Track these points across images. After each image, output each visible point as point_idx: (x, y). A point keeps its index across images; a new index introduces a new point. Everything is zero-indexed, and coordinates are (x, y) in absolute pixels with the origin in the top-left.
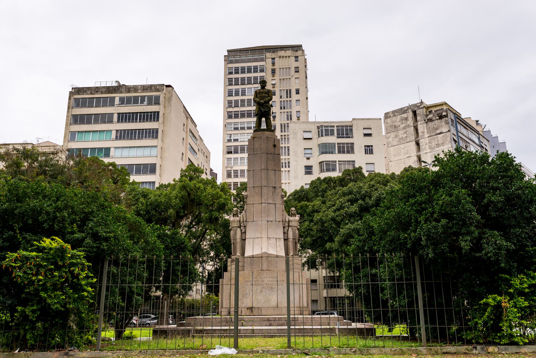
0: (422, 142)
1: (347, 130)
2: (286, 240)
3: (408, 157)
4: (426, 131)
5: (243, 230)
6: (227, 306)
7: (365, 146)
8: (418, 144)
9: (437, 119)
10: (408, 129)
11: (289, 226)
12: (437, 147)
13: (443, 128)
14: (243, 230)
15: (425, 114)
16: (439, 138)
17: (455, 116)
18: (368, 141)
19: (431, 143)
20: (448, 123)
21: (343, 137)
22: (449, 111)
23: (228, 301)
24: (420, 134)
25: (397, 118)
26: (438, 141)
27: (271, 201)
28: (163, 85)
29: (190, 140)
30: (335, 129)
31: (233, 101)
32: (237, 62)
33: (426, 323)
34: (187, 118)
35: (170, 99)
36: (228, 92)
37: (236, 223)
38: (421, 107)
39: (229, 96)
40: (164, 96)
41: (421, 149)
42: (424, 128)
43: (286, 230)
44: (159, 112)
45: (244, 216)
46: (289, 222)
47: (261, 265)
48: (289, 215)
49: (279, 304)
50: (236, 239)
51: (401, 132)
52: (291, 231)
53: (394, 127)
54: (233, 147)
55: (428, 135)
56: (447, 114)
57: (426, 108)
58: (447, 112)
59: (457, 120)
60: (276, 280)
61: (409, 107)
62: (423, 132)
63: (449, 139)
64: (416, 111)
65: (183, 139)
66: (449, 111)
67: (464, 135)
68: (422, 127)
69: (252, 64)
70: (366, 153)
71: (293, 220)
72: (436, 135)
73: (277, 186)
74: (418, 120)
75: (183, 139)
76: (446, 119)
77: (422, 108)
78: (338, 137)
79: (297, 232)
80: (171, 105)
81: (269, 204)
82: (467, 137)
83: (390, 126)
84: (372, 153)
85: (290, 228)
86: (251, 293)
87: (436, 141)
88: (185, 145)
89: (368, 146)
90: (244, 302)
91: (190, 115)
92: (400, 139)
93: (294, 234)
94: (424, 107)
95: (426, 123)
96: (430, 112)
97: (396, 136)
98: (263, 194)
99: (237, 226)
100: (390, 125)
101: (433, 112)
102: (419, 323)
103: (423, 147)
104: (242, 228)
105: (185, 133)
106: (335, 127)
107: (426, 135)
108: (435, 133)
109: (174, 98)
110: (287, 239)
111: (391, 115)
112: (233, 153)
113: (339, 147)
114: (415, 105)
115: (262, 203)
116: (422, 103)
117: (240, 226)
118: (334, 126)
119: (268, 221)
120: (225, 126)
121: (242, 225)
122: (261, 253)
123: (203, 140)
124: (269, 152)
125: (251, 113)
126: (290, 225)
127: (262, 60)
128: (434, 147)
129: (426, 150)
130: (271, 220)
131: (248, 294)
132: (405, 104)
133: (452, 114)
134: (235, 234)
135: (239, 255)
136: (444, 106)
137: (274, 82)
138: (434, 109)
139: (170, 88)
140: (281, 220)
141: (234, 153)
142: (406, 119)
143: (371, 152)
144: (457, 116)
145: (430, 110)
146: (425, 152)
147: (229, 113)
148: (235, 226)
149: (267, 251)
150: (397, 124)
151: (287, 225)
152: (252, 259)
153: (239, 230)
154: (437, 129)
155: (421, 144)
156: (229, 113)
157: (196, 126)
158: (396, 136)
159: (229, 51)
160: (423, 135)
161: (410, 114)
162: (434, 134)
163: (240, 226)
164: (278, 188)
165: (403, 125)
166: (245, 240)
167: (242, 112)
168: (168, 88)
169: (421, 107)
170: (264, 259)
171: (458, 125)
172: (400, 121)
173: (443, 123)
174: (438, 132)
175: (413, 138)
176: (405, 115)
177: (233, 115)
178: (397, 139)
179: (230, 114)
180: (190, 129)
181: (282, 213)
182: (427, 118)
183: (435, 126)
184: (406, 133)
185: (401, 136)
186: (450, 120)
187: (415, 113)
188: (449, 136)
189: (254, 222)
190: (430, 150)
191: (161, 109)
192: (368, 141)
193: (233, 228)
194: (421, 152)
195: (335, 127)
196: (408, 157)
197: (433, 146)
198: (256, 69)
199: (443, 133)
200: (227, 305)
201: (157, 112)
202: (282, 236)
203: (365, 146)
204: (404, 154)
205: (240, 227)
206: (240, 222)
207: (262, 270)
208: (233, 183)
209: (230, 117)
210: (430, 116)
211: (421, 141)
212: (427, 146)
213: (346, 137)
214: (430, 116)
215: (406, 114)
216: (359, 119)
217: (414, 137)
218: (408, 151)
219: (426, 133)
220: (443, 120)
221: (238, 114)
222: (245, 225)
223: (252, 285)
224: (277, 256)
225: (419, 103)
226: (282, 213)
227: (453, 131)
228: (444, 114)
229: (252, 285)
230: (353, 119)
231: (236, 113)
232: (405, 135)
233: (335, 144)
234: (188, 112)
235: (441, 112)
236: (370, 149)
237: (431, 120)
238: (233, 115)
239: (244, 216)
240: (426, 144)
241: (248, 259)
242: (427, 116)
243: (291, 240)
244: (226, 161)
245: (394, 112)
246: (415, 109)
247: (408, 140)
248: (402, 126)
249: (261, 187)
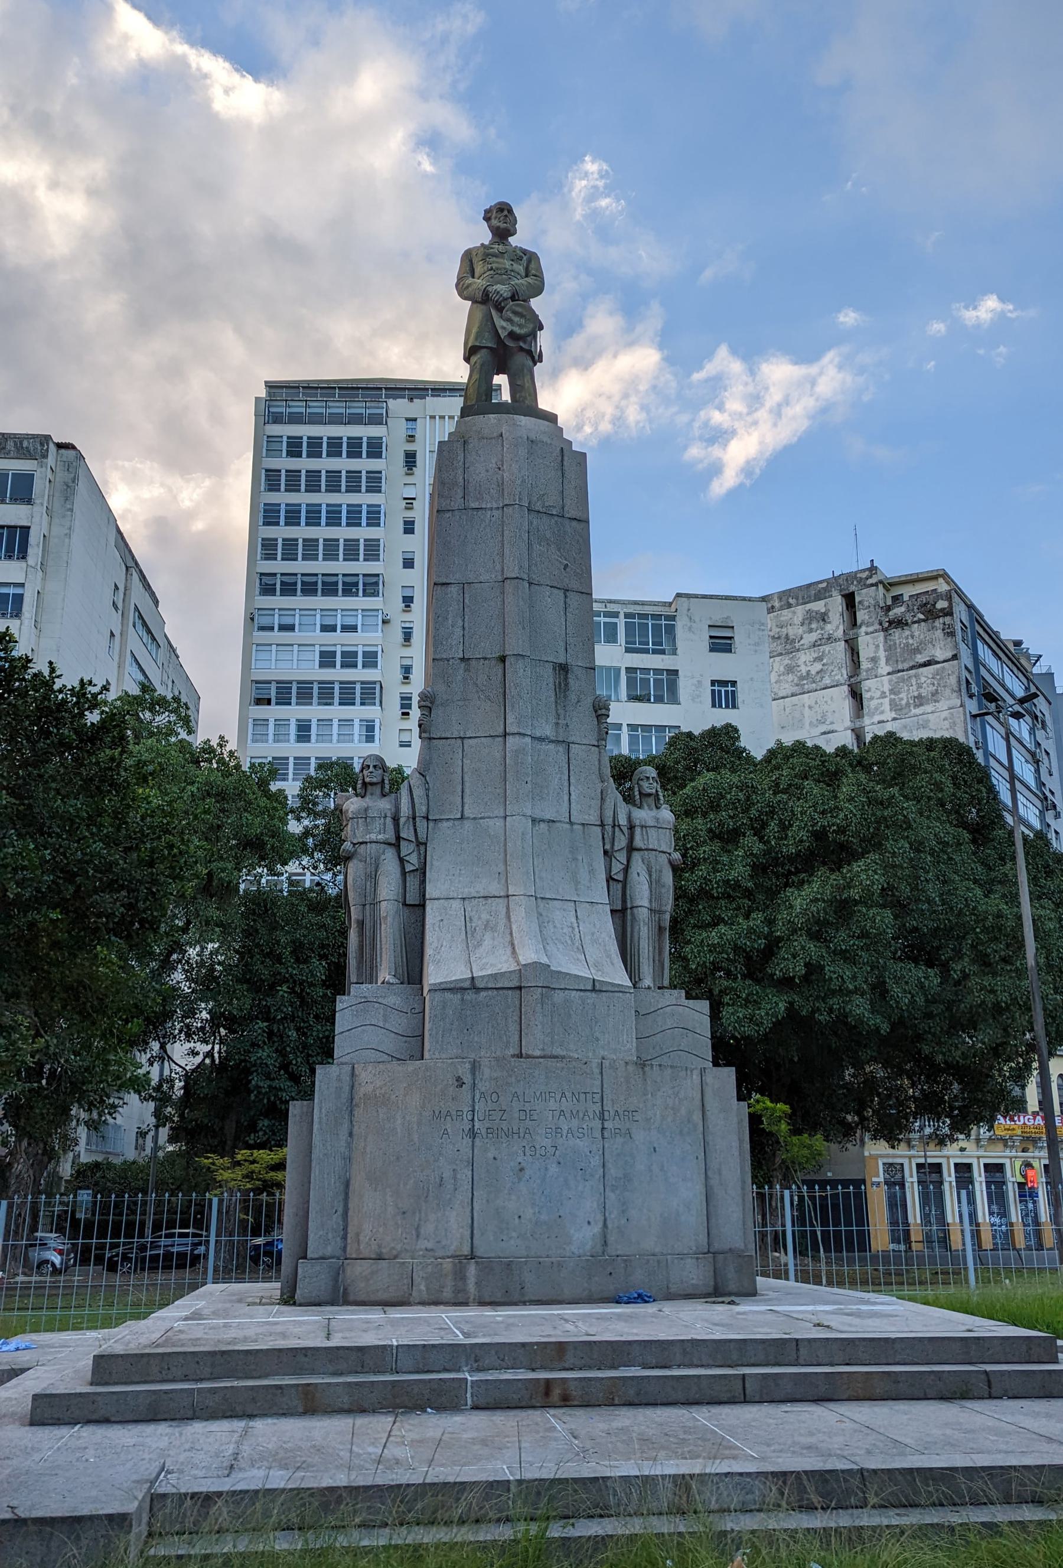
0: (871, 688)
1: (657, 628)
2: (622, 914)
3: (824, 733)
4: (882, 654)
5: (414, 859)
6: (329, 1251)
7: (713, 683)
8: (856, 695)
9: (919, 621)
10: (827, 648)
11: (631, 849)
12: (916, 706)
13: (938, 646)
15: (882, 604)
16: (923, 679)
17: (971, 615)
18: (723, 666)
19: (899, 693)
20: (952, 634)
21: (646, 651)
22: (956, 599)
24: (865, 665)
25: (794, 613)
26: (920, 686)
27: (548, 731)
28: (47, 438)
29: (135, 642)
30: (621, 622)
31: (280, 541)
32: (296, 419)
33: (784, 1232)
34: (127, 568)
35: (69, 490)
36: (265, 511)
37: (377, 824)
38: (870, 581)
39: (266, 524)
40: (49, 475)
41: (866, 710)
42: (878, 646)
43: (617, 868)
44: (29, 528)
46: (632, 828)
47: (513, 1028)
48: (628, 799)
49: (611, 1239)
50: (375, 904)
51: (804, 657)
52: (644, 878)
53: (783, 640)
54: (273, 686)
55: (889, 669)
56: (951, 606)
57: (884, 586)
58: (949, 599)
59: (978, 628)
60: (597, 1108)
61: (834, 582)
62: (874, 660)
63: (953, 680)
64: (853, 594)
65: (112, 635)
66: (956, 599)
67: (992, 675)
68: (870, 644)
69: (345, 432)
71: (651, 822)
72: (912, 668)
73: (576, 662)
74: (859, 621)
75: (112, 635)
76: (948, 620)
77: (872, 585)
78: (628, 650)
79: (668, 878)
80: (72, 510)
81: (540, 739)
82: (999, 683)
83: (773, 637)
84: (734, 707)
85: (636, 856)
87: (915, 687)
88: (116, 657)
90: (428, 1228)
91: (137, 564)
92: (802, 678)
93: (655, 883)
94: (881, 582)
95: (885, 630)
96: (897, 599)
97: (790, 669)
98: (511, 691)
99: (381, 837)
100: (772, 634)
101: (906, 598)
102: (793, 1232)
103: (873, 704)
104: (406, 848)
105: (117, 617)
106: (622, 615)
107: (884, 668)
108: (912, 664)
109: (82, 487)
110: (624, 910)
111: (777, 604)
112: (273, 701)
113: (631, 683)
114: (851, 577)
115: (505, 735)
116: (873, 569)
117: (398, 838)
118: (616, 615)
119: (534, 820)
120: (252, 619)
121: (406, 833)
122: (513, 967)
123: (178, 652)
124: (538, 507)
125: (336, 584)
126: (638, 842)
127: (376, 420)
128: (908, 704)
129: (882, 712)
130: (548, 817)
132: (819, 572)
133: (963, 607)
134: (373, 877)
135: (388, 978)
136: (941, 580)
137: (410, 492)
138: (907, 591)
139: (71, 452)
142: (823, 618)
143: (732, 702)
144: (976, 616)
145: (896, 591)
146: (876, 719)
147: (265, 579)
148: (373, 837)
149: (544, 960)
150: (792, 632)
151: (621, 842)
152: (470, 996)
154: (917, 651)
155: (866, 696)
156: (265, 579)
157: (156, 602)
158: (790, 669)
159: (270, 386)
160: (876, 667)
161: (836, 603)
162: (906, 666)
163: (398, 838)
164: (579, 672)
165: (814, 637)
166: (422, 906)
167: (306, 579)
168: (63, 451)
169: (870, 581)
170: (532, 998)
171: (979, 644)
172: (802, 624)
173: (939, 633)
174: (921, 658)
175: (842, 675)
176: (819, 606)
177: (278, 587)
178: (790, 677)
179: (266, 580)
180: (136, 608)
181: (599, 786)
182: (886, 615)
183: (911, 641)
184: (819, 659)
185: (804, 669)
186: (960, 624)
187: (850, 600)
188: (952, 674)
189: (467, 824)
190: (893, 715)
191: (36, 519)
192: (723, 666)
193: (362, 849)
194: (866, 717)
195: (622, 615)
196: (824, 733)
197: (904, 702)
198: (354, 448)
199: (938, 663)
201: (21, 527)
202: (600, 893)
203: (713, 683)
204: (811, 723)
205: (396, 843)
206: (396, 820)
209: (268, 590)
210: (898, 611)
211: (866, 685)
212: (887, 701)
213: (655, 652)
214: (898, 611)
215: (822, 602)
216: (696, 596)
217: (845, 672)
218: (824, 716)
219: (883, 661)
220: (939, 623)
221: (295, 584)
222: (422, 836)
223: (473, 1134)
224: (595, 987)
225: (864, 570)
227: (966, 659)
228: (942, 604)
229: (473, 1134)
230: (678, 595)
231: (286, 579)
232: (818, 666)
233: (618, 670)
234: (130, 551)
235: (931, 598)
236: (727, 692)
237: (899, 623)
238: (278, 587)
240: (883, 695)
241: (448, 995)
242: (888, 609)
243: (643, 914)
244: (250, 726)
245: (784, 595)
246: (852, 588)
247: (827, 681)
248: (810, 638)
249: (503, 659)
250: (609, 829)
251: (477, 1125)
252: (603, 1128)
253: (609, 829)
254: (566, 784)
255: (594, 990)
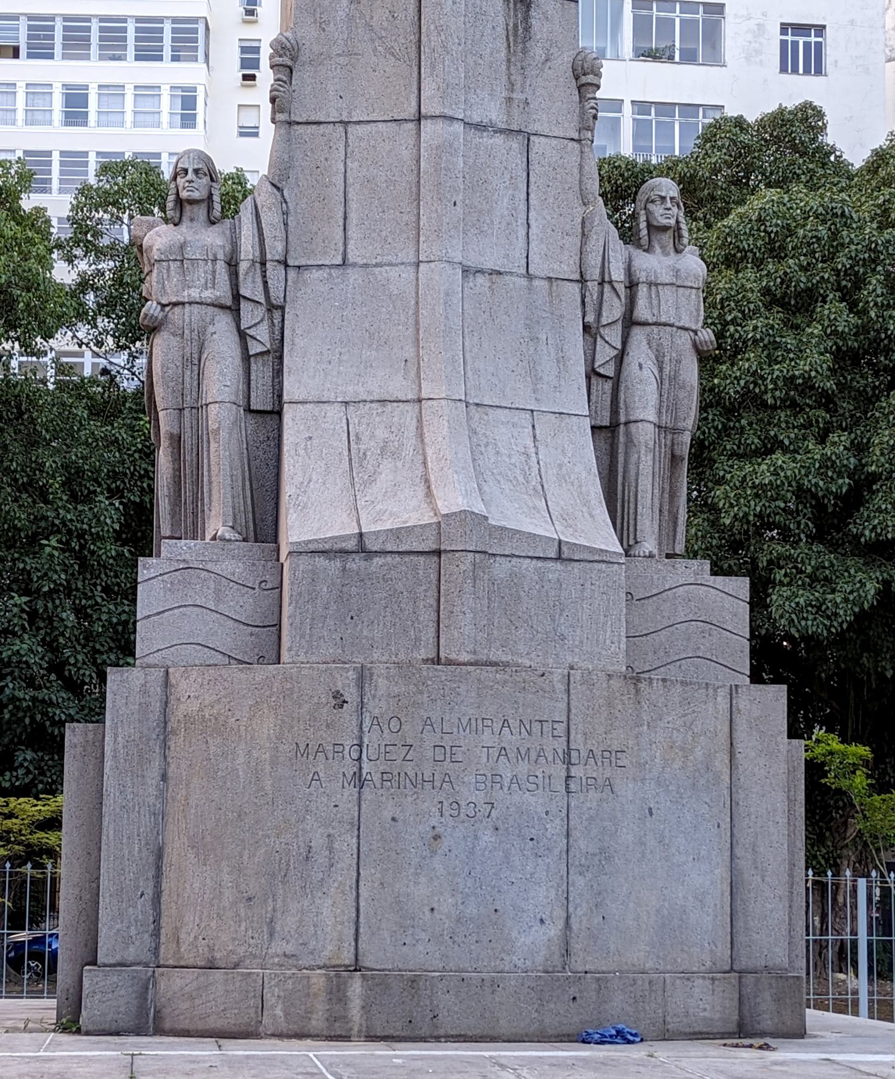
6: (131, 953)
11: (629, 322)
14: (262, 334)
23: (142, 908)
37: (201, 273)
43: (605, 354)
45: (270, 219)
46: (632, 286)
47: (427, 616)
49: (577, 946)
50: (199, 408)
52: (650, 366)
54: (23, 24)
70: (783, 69)
79: (691, 372)
81: (480, 127)
84: (819, 72)
85: (638, 335)
86: (346, 843)
89: (801, 29)
98: (431, 40)
104: (250, 315)
112: (23, 52)
117: (237, 297)
119: (466, 271)
121: (250, 288)
122: (428, 518)
126: (642, 311)
130: (489, 265)
131: (321, 859)
135: (223, 531)
140: (568, 268)
141: (30, 56)
149: (479, 508)
151: (614, 310)
152: (356, 563)
153: (223, 323)
163: (237, 297)
181: (579, 211)
189: (354, 276)
200: (127, 941)
206: (232, 265)
207: (437, 661)
208: (63, 153)
222: (276, 294)
223: (359, 781)
226: (579, 211)
229: (359, 781)
236: (807, 45)
239: (270, 219)
243: (645, 434)
250: (593, 286)
251: (366, 767)
252: (568, 777)
253: (593, 286)
254: (523, 207)
255: (559, 558)
